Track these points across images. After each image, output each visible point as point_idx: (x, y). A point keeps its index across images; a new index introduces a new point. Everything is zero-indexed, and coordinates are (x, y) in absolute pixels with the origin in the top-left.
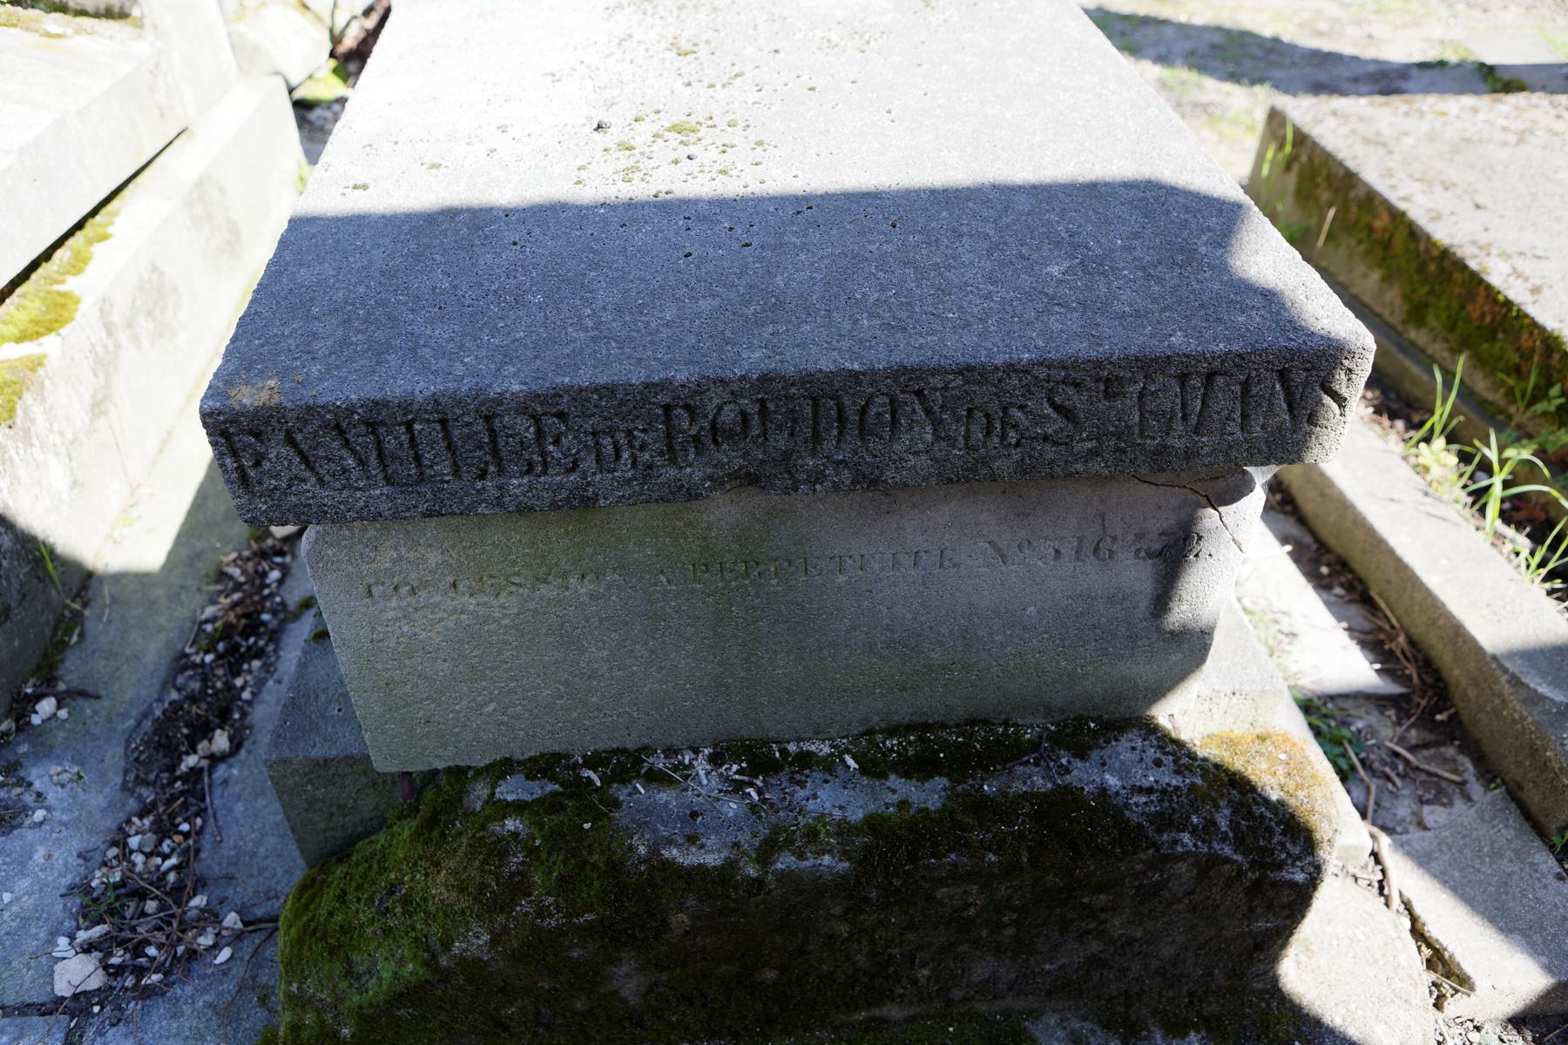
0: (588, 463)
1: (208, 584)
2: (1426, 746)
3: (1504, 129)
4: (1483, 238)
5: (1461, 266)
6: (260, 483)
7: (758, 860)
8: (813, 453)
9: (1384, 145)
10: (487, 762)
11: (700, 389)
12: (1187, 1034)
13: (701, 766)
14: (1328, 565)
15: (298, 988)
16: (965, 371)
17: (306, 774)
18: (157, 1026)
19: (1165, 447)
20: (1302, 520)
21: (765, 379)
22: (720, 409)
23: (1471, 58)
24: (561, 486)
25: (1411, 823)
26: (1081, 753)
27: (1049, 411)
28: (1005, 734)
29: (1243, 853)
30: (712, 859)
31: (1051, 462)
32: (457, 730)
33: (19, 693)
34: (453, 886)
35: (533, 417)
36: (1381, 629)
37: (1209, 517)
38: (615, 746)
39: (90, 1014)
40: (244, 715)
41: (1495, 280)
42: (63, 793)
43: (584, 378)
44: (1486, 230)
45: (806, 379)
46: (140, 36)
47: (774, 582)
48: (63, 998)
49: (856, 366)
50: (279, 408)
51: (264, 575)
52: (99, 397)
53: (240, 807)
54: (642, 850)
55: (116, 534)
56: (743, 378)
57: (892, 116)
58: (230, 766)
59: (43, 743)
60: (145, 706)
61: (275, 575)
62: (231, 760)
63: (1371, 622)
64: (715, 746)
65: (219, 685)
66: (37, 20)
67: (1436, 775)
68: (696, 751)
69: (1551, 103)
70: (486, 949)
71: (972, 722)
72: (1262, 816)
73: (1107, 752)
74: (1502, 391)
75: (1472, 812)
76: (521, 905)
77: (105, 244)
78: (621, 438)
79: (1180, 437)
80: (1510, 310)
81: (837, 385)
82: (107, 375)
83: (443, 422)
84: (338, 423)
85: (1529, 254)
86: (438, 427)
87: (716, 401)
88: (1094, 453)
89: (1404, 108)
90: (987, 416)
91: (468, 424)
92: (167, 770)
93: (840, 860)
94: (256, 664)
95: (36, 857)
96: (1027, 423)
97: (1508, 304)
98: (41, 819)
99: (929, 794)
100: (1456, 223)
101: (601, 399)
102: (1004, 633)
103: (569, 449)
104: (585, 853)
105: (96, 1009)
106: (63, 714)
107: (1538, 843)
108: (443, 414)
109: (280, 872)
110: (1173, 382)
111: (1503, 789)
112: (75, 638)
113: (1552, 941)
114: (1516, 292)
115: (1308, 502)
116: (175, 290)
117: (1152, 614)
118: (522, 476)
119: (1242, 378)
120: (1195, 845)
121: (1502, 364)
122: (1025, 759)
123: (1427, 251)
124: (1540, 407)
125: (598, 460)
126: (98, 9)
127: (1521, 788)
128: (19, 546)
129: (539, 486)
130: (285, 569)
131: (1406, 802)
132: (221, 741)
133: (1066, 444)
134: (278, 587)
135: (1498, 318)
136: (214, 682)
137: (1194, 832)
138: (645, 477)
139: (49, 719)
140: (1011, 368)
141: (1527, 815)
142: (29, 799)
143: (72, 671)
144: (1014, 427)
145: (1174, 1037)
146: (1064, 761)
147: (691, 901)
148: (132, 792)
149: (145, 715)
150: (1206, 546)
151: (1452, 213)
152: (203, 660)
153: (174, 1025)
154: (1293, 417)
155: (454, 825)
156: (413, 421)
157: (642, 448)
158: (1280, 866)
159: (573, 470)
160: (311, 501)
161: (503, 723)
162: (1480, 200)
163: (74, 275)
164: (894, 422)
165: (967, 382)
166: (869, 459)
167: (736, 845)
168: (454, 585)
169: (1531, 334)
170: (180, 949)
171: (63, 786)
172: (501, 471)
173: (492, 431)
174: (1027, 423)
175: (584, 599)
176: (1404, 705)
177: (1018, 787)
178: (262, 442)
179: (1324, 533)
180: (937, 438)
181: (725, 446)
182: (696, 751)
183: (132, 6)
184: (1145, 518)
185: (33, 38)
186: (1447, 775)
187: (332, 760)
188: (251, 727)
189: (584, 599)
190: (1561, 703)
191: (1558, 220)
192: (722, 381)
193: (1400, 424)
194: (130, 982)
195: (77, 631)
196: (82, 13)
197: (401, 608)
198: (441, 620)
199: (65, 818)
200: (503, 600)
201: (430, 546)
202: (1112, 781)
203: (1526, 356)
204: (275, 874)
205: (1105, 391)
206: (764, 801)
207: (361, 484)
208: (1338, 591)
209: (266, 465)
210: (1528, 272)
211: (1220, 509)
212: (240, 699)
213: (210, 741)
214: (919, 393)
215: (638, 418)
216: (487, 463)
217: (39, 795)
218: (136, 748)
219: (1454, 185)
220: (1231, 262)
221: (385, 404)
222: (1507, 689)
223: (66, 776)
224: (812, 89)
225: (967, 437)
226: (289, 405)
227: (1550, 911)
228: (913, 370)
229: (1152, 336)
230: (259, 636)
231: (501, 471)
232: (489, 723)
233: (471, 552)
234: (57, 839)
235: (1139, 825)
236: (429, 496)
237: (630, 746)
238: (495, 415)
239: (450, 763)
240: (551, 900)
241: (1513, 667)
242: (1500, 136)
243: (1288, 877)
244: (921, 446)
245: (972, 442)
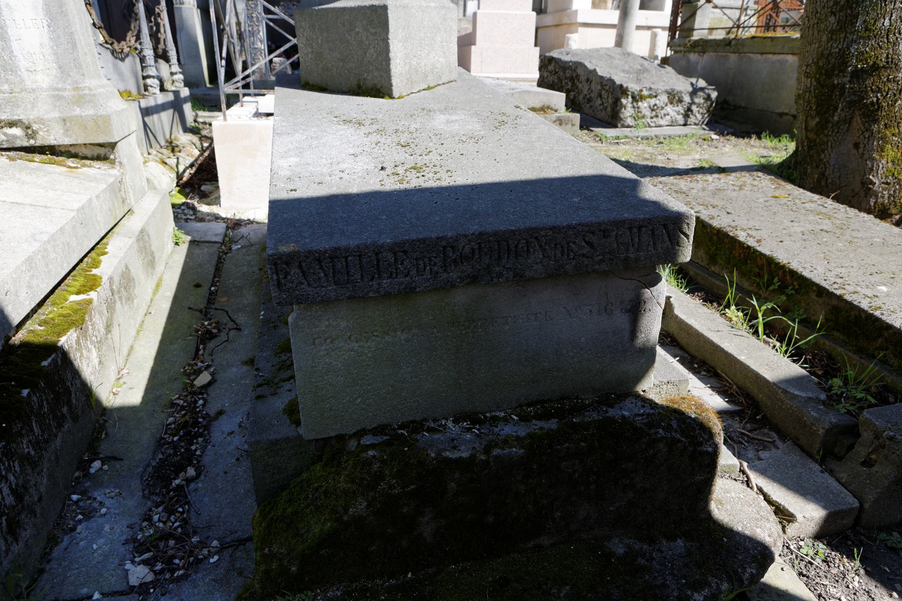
0: (413, 272)
1: (167, 409)
2: (755, 430)
3: (733, 185)
4: (733, 224)
5: (726, 235)
6: (285, 286)
7: (485, 453)
8: (498, 266)
9: (684, 193)
10: (354, 431)
11: (457, 240)
12: (676, 540)
13: (450, 424)
14: (697, 364)
15: (269, 551)
16: (553, 228)
17: (266, 449)
18: (187, 592)
19: (628, 257)
20: (682, 348)
21: (481, 234)
22: (464, 247)
23: (714, 165)
24: (402, 283)
25: (755, 459)
26: (611, 406)
27: (584, 244)
28: (577, 402)
29: (685, 437)
30: (465, 455)
31: (587, 265)
32: (343, 414)
33: (82, 459)
34: (348, 481)
35: (393, 253)
36: (725, 386)
37: (647, 292)
38: (411, 419)
39: (150, 593)
40: (199, 462)
41: (741, 239)
42: (113, 501)
43: (414, 236)
44: (734, 221)
45: (496, 234)
46: (113, 168)
47: (480, 330)
48: (135, 587)
49: (513, 228)
50: (299, 251)
51: (196, 402)
52: (109, 323)
53: (206, 499)
54: (433, 455)
55: (114, 391)
56: (473, 234)
57: (497, 161)
58: (197, 483)
59: (97, 481)
60: (146, 462)
61: (201, 402)
62: (196, 481)
63: (720, 383)
64: (454, 417)
65: (183, 450)
66: (64, 161)
67: (763, 440)
68: (447, 419)
69: (750, 175)
70: (365, 510)
71: (563, 398)
72: (689, 422)
73: (621, 405)
74: (755, 285)
75: (780, 451)
76: (381, 485)
77: (105, 256)
78: (426, 260)
79: (632, 253)
80: (750, 250)
81: (507, 236)
82: (112, 314)
83: (360, 256)
84: (318, 257)
85: (753, 228)
86: (358, 258)
87: (463, 244)
88: (602, 261)
89: (689, 179)
90: (562, 247)
91: (370, 256)
92: (164, 487)
93: (520, 449)
94: (200, 439)
95: (105, 529)
96: (576, 249)
97: (749, 247)
98: (105, 512)
99: (553, 424)
100: (721, 219)
101: (420, 244)
102: (573, 351)
103: (407, 266)
104: (407, 460)
105: (152, 590)
106: (106, 467)
107: (810, 460)
108: (359, 252)
109: (235, 523)
110: (627, 230)
111: (791, 441)
112: (103, 436)
113: (824, 496)
114: (751, 243)
115: (682, 339)
116: (133, 279)
117: (631, 339)
118: (387, 279)
119: (651, 228)
120: (665, 434)
121: (752, 274)
122: (588, 409)
123: (711, 232)
124: (771, 288)
125: (417, 271)
126: (93, 156)
127: (798, 439)
128: (82, 387)
129: (394, 283)
130: (205, 401)
131: (751, 452)
132: (191, 472)
133: (591, 257)
134: (203, 408)
135: (746, 254)
136: (180, 450)
137: (663, 428)
138: (435, 277)
139: (98, 470)
140: (569, 227)
141: (803, 450)
142: (96, 505)
143: (105, 449)
144: (572, 251)
145: (671, 541)
146: (605, 409)
147: (457, 476)
148: (149, 499)
149: (148, 466)
150: (648, 306)
151: (718, 216)
152: (173, 440)
153: (196, 591)
154: (672, 244)
155: (343, 458)
156: (348, 256)
157: (435, 264)
158: (701, 444)
159: (406, 276)
160: (304, 293)
161: (364, 409)
162: (728, 210)
163: (95, 268)
164: (528, 251)
165: (554, 233)
166: (519, 267)
167: (474, 448)
168: (350, 338)
169: (761, 258)
170: (191, 559)
171: (112, 498)
172: (380, 277)
173: (378, 260)
174: (576, 249)
175: (403, 342)
176: (742, 414)
177: (587, 419)
178: (289, 267)
179: (692, 351)
180: (544, 257)
181: (465, 264)
182: (447, 419)
183: (110, 155)
184: (623, 294)
185: (64, 169)
186: (766, 439)
187: (279, 440)
188: (204, 466)
189: (403, 342)
190: (805, 397)
191: (762, 216)
192: (465, 235)
193: (715, 304)
194: (168, 576)
195: (104, 433)
196: (86, 158)
197: (326, 349)
198: (343, 355)
199: (116, 511)
200: (369, 344)
201: (342, 318)
202: (626, 413)
203: (761, 268)
204: (232, 523)
205: (603, 235)
206: (482, 433)
207: (325, 284)
208: (703, 373)
209: (289, 277)
210: (754, 235)
211: (651, 289)
212: (196, 455)
213: (185, 472)
214: (536, 238)
215: (433, 252)
216: (375, 273)
217: (101, 503)
218: (147, 479)
219: (717, 206)
220: (639, 195)
221: (339, 249)
222: (782, 396)
223: (113, 494)
224: (462, 154)
225: (555, 256)
226: (303, 251)
227: (821, 485)
228: (534, 229)
229: (616, 215)
230: (199, 428)
231: (380, 277)
232: (357, 409)
233: (358, 321)
234: (114, 521)
235: (641, 427)
236: (351, 289)
237: (418, 419)
238: (380, 252)
239: (338, 433)
240: (394, 481)
241: (783, 386)
242: (731, 187)
243: (705, 449)
244: (538, 260)
245: (557, 258)
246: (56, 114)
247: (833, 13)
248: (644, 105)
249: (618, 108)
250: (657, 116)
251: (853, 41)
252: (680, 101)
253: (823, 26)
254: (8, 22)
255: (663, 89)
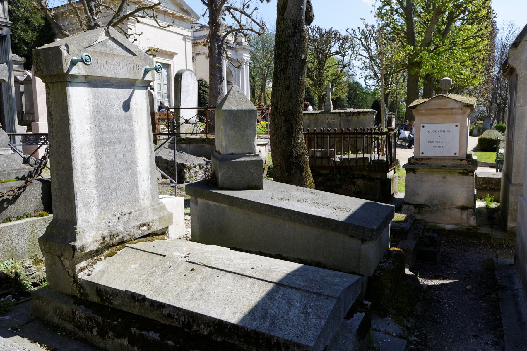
246: (156, 218)
247: (284, 139)
248: (192, 171)
249: (183, 174)
250: (197, 176)
251: (293, 148)
252: (203, 168)
253: (282, 142)
254: (139, 179)
255: (197, 163)
